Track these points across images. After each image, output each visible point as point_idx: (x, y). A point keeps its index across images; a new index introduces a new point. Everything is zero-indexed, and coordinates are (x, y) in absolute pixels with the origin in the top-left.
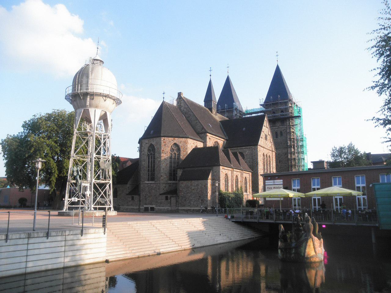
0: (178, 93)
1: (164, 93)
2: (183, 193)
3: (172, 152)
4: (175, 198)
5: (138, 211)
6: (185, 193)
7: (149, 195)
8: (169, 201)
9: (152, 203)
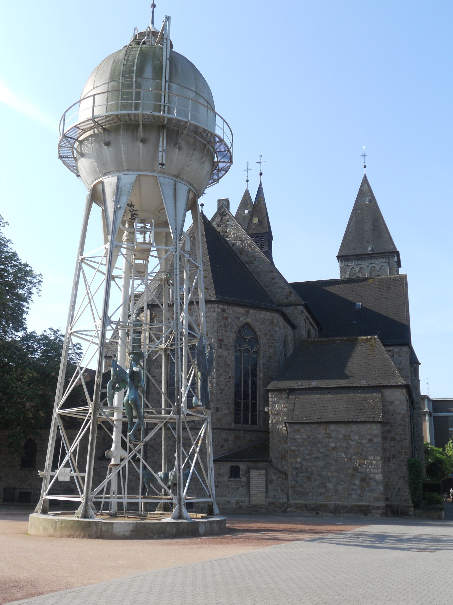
0: (219, 201)
2: (299, 460)
3: (240, 347)
4: (263, 472)
6: (307, 457)
8: (244, 479)
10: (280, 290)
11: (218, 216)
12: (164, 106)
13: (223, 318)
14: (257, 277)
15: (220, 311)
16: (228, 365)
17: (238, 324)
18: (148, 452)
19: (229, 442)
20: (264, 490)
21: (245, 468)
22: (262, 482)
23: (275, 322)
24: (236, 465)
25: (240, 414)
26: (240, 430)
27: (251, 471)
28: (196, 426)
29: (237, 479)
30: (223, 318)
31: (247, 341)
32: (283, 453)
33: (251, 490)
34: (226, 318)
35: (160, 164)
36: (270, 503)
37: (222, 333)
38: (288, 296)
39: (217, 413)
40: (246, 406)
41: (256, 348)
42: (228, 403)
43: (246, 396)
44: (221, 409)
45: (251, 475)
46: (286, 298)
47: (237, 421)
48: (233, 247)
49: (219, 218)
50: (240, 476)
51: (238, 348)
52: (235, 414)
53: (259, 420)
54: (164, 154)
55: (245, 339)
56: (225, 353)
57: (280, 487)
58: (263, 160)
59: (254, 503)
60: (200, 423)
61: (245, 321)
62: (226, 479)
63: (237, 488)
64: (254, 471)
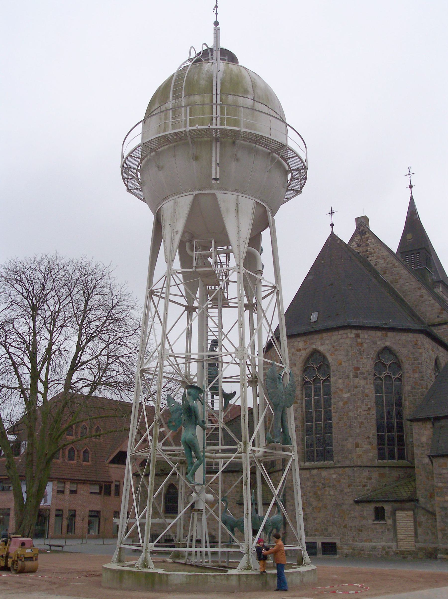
0: (357, 219)
1: (332, 213)
4: (410, 513)
5: (225, 547)
7: (315, 504)
8: (390, 522)
9: (326, 529)
10: (430, 309)
11: (357, 235)
12: (216, 118)
13: (358, 344)
14: (404, 297)
15: (353, 336)
16: (367, 396)
17: (375, 349)
18: (287, 494)
19: (372, 481)
20: (413, 533)
21: (391, 509)
22: (410, 524)
23: (419, 343)
24: (380, 506)
25: (384, 449)
26: (384, 467)
27: (397, 512)
28: (335, 464)
29: (382, 522)
30: (358, 344)
31: (388, 366)
32: (432, 491)
33: (398, 533)
34: (361, 344)
35: (214, 179)
36: (420, 549)
37: (357, 361)
38: (440, 313)
39: (357, 449)
40: (391, 440)
41: (399, 374)
42: (369, 437)
43: (390, 429)
44: (361, 444)
45: (397, 517)
46: (438, 317)
47: (381, 456)
48: (375, 267)
49: (359, 238)
50: (385, 518)
51: (378, 376)
52: (379, 449)
53: (407, 455)
54: (218, 168)
55: (385, 366)
56: (362, 382)
57: (430, 529)
58: (412, 172)
59: (403, 549)
60: (339, 460)
61: (383, 346)
62: (370, 522)
63: (382, 532)
64: (401, 512)
